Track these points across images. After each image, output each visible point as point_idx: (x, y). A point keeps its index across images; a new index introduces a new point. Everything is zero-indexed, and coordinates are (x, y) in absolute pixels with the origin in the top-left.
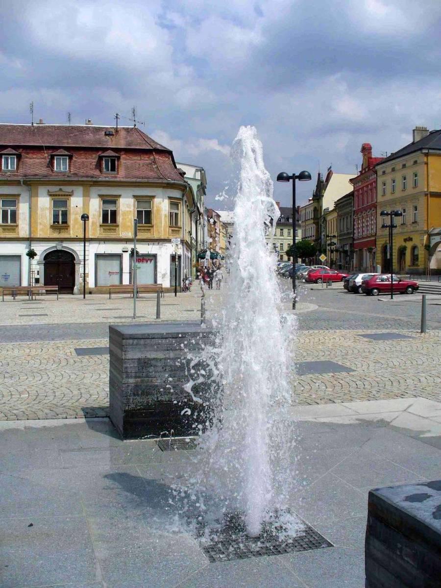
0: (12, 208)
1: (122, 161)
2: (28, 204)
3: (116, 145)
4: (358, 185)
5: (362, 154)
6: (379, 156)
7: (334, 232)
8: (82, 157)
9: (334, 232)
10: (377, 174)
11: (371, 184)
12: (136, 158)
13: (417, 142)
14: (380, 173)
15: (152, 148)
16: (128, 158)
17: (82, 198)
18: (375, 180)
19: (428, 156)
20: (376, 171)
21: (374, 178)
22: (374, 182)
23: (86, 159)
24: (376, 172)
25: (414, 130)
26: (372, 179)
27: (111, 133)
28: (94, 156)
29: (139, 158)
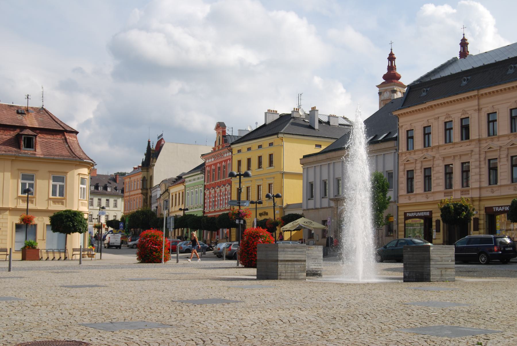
0: (61, 183)
1: (38, 139)
2: (302, 181)
3: (11, 123)
4: (210, 160)
5: (216, 131)
6: (236, 133)
7: (179, 204)
9: (179, 204)
10: (232, 152)
11: (226, 161)
12: (49, 137)
13: (269, 124)
14: (235, 151)
15: (63, 129)
16: (42, 136)
17: (10, 173)
18: (230, 157)
19: (480, 197)
20: (232, 150)
21: (229, 156)
22: (229, 159)
23: (5, 135)
24: (231, 151)
25: (266, 113)
26: (227, 156)
27: (23, 112)
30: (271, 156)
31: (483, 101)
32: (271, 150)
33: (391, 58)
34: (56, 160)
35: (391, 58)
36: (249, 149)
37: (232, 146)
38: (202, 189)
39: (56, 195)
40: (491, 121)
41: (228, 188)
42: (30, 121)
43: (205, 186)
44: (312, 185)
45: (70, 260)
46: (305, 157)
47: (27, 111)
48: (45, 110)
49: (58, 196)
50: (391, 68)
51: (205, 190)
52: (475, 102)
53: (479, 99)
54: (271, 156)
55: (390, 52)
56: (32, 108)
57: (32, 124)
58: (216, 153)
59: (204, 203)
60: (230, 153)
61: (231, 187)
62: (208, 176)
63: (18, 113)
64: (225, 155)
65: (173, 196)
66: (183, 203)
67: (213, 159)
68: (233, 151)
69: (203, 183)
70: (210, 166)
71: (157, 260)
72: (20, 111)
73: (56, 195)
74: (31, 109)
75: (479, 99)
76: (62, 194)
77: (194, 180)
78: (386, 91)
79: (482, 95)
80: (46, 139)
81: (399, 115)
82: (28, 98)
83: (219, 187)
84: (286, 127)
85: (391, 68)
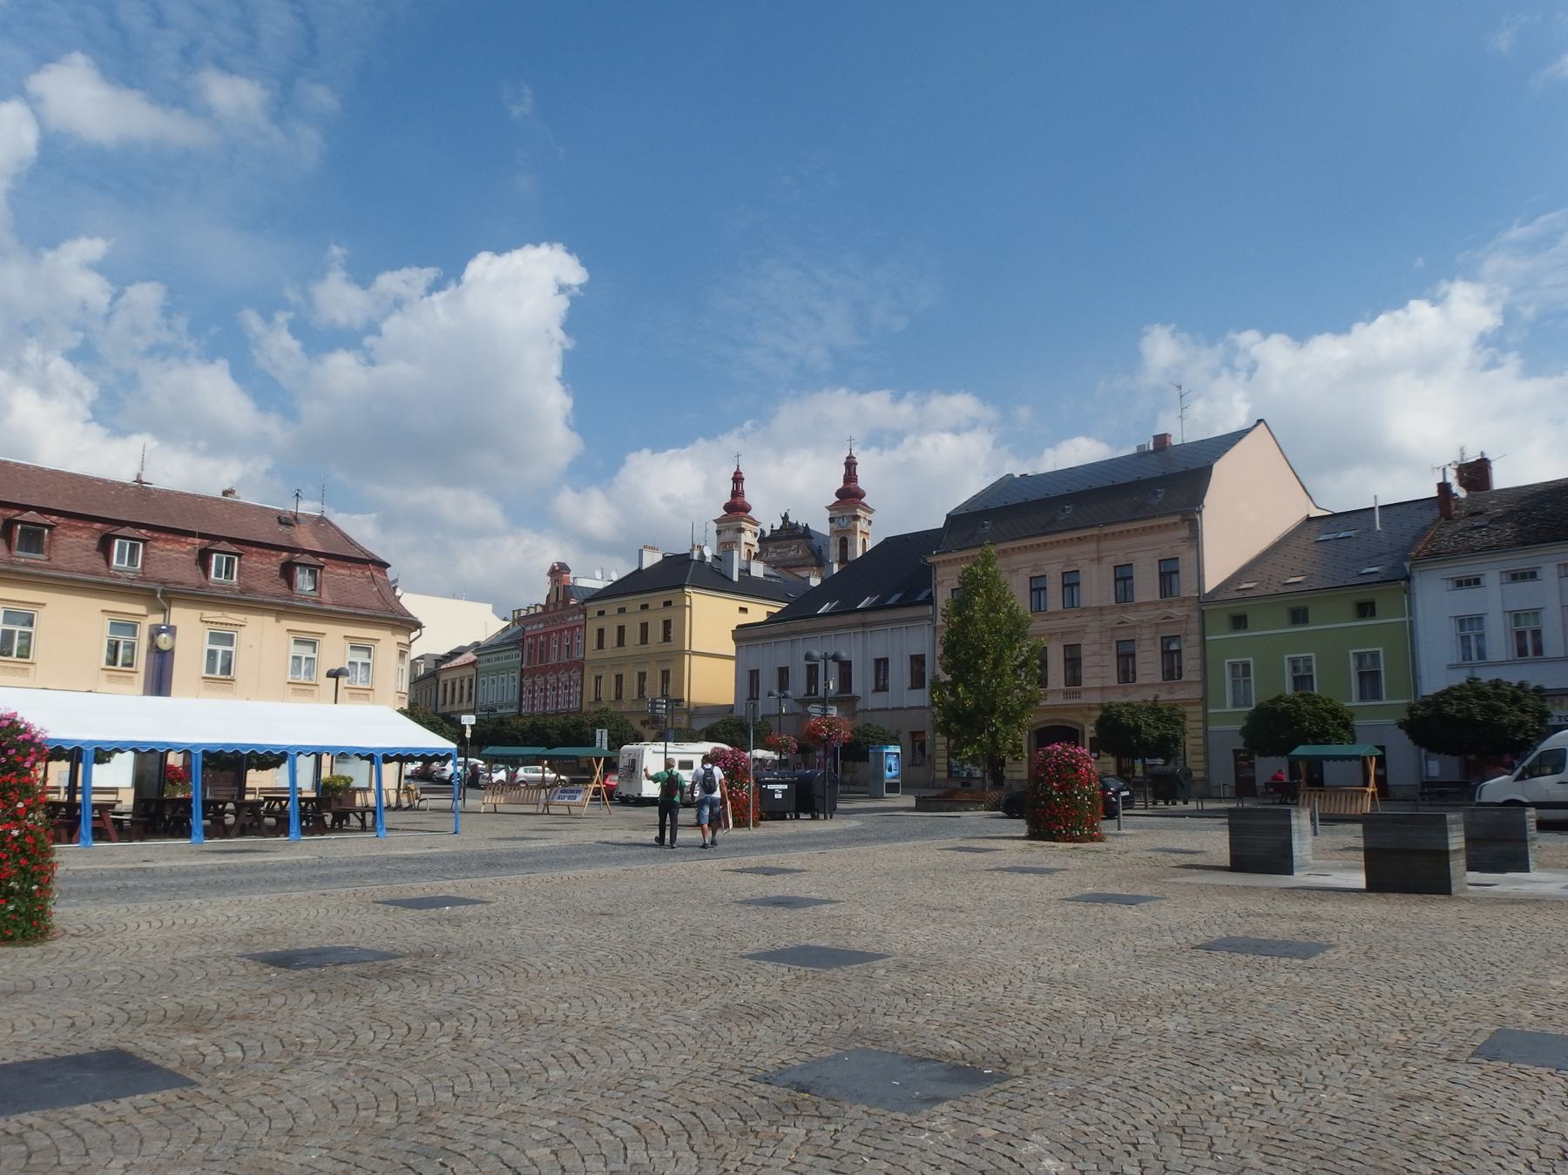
8: (254, 559)
18: (583, 623)
22: (580, 627)
23: (262, 563)
28: (274, 559)
29: (348, 572)
30: (667, 624)
31: (1105, 545)
32: (668, 614)
33: (738, 479)
34: (335, 612)
35: (738, 479)
36: (645, 607)
37: (587, 605)
38: (517, 675)
39: (214, 673)
40: (1068, 585)
41: (576, 676)
42: (306, 539)
43: (522, 670)
44: (754, 675)
45: (406, 809)
46: (738, 627)
47: (295, 518)
48: (325, 519)
49: (218, 674)
50: (737, 493)
51: (522, 677)
52: (1091, 547)
53: (1098, 541)
54: (667, 624)
55: (735, 470)
56: (302, 514)
57: (310, 546)
58: (547, 616)
59: (521, 699)
60: (582, 616)
61: (582, 675)
62: (529, 653)
63: (281, 522)
64: (570, 619)
65: (445, 685)
66: (470, 699)
67: (541, 626)
68: (588, 611)
69: (519, 665)
70: (536, 637)
71: (1436, 883)
72: (283, 520)
73: (214, 673)
74: (302, 518)
75: (1098, 541)
76: (227, 669)
77: (498, 659)
78: (729, 528)
79: (1106, 535)
80: (337, 574)
81: (938, 562)
82: (297, 495)
83: (556, 672)
84: (690, 574)
85: (737, 493)
